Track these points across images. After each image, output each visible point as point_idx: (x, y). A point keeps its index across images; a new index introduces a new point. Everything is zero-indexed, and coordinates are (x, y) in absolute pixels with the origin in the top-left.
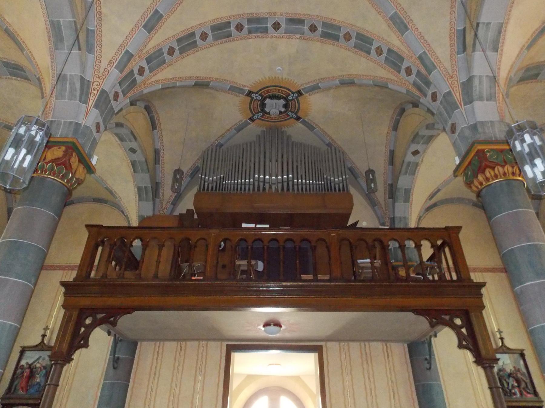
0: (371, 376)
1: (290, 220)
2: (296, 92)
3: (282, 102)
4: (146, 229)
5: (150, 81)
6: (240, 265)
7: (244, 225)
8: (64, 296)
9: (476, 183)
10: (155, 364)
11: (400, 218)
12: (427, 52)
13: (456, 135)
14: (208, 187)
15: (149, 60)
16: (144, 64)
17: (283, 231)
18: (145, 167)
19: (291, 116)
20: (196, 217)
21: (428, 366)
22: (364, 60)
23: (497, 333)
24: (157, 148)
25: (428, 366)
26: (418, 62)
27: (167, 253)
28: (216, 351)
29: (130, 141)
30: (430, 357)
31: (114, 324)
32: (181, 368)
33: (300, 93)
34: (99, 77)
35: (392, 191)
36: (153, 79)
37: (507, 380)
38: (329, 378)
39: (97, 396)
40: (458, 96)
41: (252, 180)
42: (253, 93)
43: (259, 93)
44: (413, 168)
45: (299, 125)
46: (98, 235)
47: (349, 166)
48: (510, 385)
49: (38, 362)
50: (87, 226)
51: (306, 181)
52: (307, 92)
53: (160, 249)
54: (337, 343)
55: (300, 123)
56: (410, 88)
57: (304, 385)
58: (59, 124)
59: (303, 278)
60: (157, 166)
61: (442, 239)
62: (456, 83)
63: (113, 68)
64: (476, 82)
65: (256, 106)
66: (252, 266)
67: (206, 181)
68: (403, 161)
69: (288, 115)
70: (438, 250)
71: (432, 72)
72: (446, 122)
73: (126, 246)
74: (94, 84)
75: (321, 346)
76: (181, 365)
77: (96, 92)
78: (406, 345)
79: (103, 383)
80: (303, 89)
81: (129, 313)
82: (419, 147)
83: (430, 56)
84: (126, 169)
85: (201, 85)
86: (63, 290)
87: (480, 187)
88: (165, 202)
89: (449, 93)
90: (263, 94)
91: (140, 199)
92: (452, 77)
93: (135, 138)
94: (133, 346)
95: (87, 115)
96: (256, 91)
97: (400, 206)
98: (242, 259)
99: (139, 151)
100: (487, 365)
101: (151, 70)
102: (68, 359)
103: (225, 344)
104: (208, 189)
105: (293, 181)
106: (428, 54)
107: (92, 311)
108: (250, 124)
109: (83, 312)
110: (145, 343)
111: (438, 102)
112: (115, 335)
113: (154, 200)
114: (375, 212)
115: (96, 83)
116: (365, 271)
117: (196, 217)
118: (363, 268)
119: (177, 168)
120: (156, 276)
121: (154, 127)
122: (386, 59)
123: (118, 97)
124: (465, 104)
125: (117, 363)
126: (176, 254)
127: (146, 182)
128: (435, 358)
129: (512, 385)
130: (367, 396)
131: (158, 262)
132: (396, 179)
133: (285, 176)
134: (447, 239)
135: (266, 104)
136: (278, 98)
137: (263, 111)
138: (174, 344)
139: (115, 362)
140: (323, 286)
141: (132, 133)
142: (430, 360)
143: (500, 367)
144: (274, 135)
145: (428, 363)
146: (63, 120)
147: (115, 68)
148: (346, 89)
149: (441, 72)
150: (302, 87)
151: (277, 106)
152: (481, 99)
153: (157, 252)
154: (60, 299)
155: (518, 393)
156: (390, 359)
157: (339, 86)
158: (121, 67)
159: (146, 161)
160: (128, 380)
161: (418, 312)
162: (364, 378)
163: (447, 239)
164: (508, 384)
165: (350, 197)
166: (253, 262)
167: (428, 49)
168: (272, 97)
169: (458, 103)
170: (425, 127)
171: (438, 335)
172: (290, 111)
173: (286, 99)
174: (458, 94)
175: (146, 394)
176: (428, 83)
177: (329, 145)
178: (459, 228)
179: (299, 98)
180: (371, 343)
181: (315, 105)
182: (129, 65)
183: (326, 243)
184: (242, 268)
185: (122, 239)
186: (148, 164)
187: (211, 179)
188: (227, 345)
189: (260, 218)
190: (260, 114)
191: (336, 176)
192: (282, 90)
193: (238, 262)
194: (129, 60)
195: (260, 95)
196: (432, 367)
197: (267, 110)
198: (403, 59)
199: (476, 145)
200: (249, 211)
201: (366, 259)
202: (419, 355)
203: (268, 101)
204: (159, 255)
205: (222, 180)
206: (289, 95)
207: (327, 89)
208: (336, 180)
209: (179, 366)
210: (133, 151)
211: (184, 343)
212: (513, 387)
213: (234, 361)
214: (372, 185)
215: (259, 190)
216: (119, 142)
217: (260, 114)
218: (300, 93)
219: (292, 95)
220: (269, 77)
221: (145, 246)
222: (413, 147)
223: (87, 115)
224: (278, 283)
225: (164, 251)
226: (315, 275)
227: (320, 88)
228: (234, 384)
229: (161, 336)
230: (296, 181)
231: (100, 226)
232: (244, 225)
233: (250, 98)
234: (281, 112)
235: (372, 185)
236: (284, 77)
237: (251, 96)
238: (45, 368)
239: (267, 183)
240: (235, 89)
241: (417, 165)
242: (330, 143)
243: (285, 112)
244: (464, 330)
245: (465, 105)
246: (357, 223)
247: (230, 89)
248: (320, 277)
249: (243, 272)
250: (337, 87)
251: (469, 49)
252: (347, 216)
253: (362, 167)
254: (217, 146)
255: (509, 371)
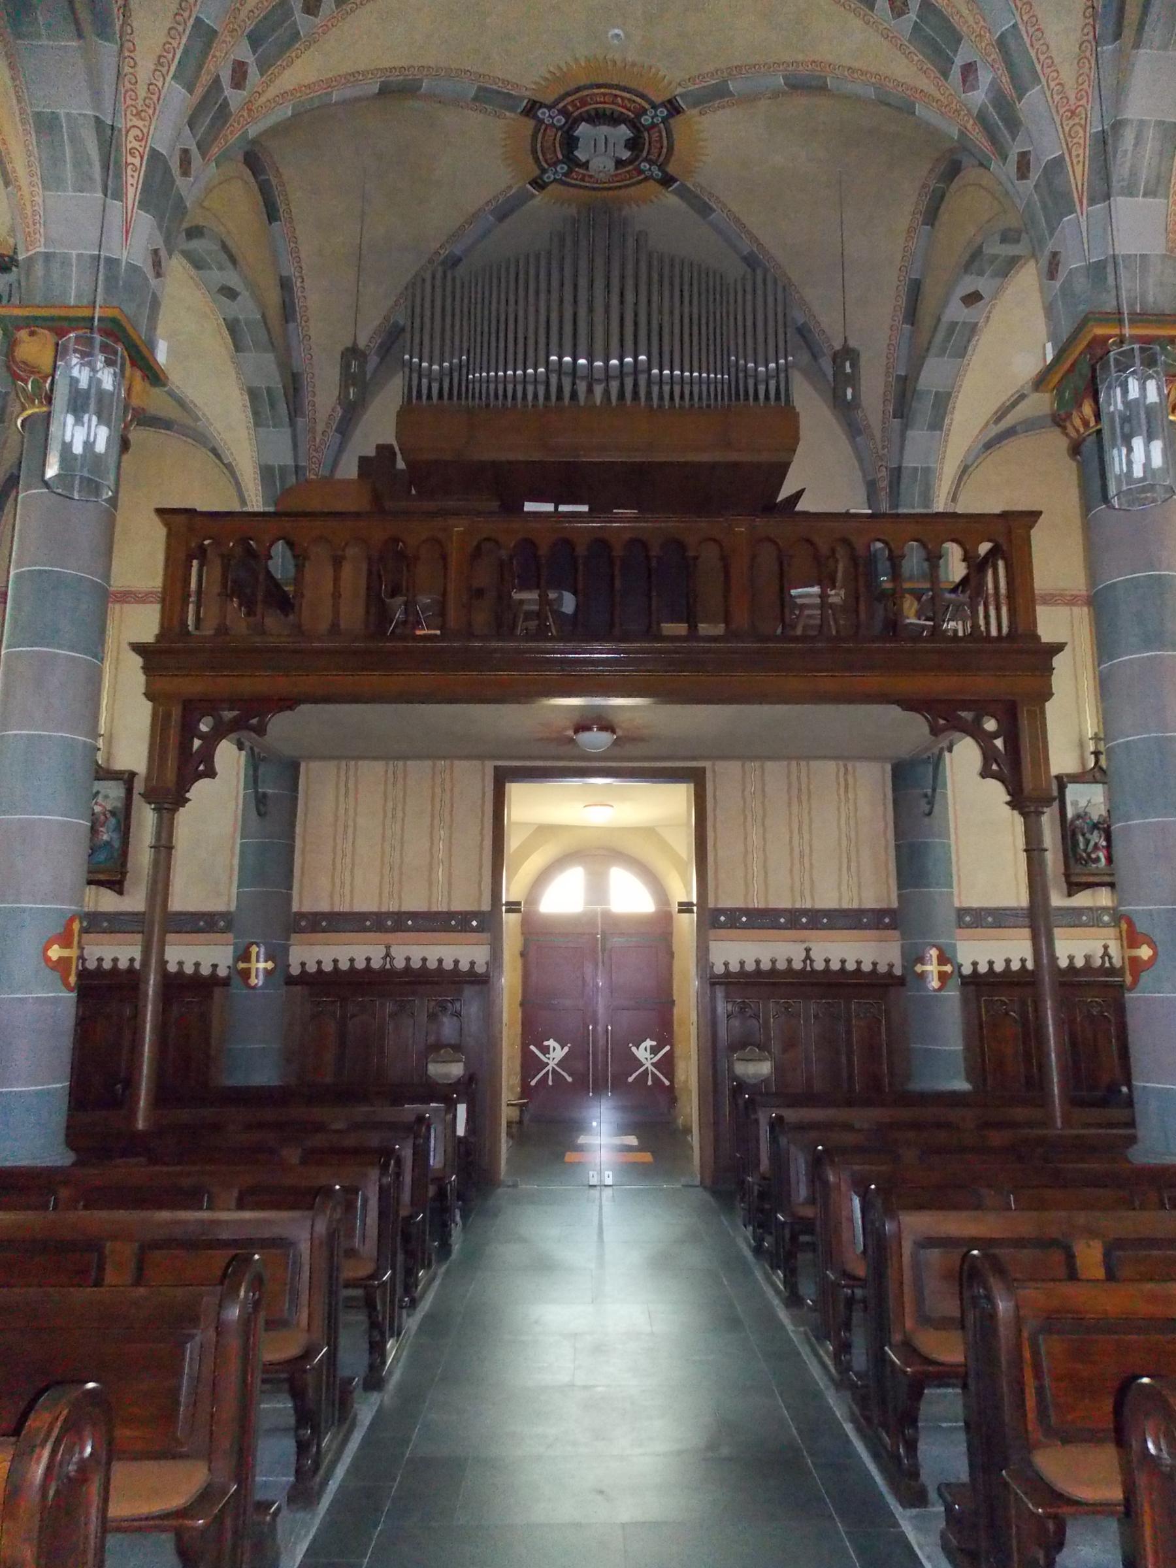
0: (805, 827)
1: (637, 483)
2: (663, 105)
3: (624, 131)
4: (295, 514)
5: (263, 99)
6: (521, 602)
7: (529, 507)
8: (145, 673)
9: (1077, 422)
10: (342, 806)
11: (916, 469)
12: (1022, 28)
13: (1057, 284)
14: (430, 388)
15: (255, 40)
16: (244, 52)
17: (623, 521)
18: (263, 336)
19: (648, 173)
20: (401, 464)
21: (927, 808)
22: (856, 23)
23: (1091, 743)
24: (285, 274)
25: (927, 808)
26: (995, 55)
27: (353, 576)
28: (473, 779)
29: (221, 268)
30: (934, 790)
31: (261, 730)
32: (400, 814)
33: (674, 108)
34: (138, 114)
35: (904, 398)
36: (272, 92)
37: (1088, 835)
38: (715, 831)
39: (232, 869)
40: (1078, 174)
41: (541, 370)
42: (542, 105)
43: (561, 105)
44: (961, 340)
45: (670, 199)
46: (189, 531)
47: (801, 321)
48: (1092, 844)
49: (96, 803)
50: (160, 512)
51: (682, 372)
52: (695, 105)
53: (337, 562)
54: (739, 763)
55: (673, 192)
56: (969, 126)
57: (665, 847)
58: (65, 261)
59: (665, 633)
60: (291, 326)
61: (989, 541)
62: (1081, 134)
63: (168, 79)
64: (1129, 135)
65: (550, 144)
66: (549, 603)
67: (425, 372)
68: (939, 320)
69: (640, 172)
70: (977, 567)
71: (1027, 90)
72: (1041, 242)
73: (253, 558)
74: (131, 137)
75: (704, 770)
76: (400, 807)
77: (137, 161)
78: (889, 767)
79: (242, 844)
80: (681, 95)
81: (290, 708)
82: (981, 284)
83: (1027, 40)
84: (217, 343)
85: (397, 90)
86: (138, 661)
87: (1082, 430)
88: (320, 428)
89: (1058, 162)
90: (570, 108)
91: (258, 420)
92: (1073, 113)
93: (233, 260)
94: (292, 769)
95: (127, 232)
96: (549, 99)
97: (917, 436)
98: (524, 587)
99: (245, 294)
100: (1032, 809)
101: (264, 66)
102: (181, 800)
103: (490, 765)
104: (429, 397)
105: (650, 374)
106: (1024, 33)
107: (208, 705)
108: (533, 196)
109: (192, 709)
110: (315, 765)
111: (1030, 183)
112: (252, 749)
113: (292, 424)
114: (856, 449)
115: (134, 132)
116: (807, 612)
117: (401, 464)
118: (803, 607)
119: (349, 345)
120: (334, 628)
121: (272, 213)
122: (916, 28)
123: (190, 163)
124: (1092, 201)
125: (265, 805)
126: (373, 578)
127: (271, 377)
128: (945, 796)
129: (1096, 844)
130: (792, 865)
131: (334, 596)
132: (917, 363)
133: (629, 360)
134: (1004, 538)
135: (578, 139)
136: (614, 120)
137: (572, 162)
138: (379, 766)
139: (260, 803)
140: (709, 651)
141: (225, 247)
142: (933, 796)
143: (1081, 811)
144: (599, 226)
145: (928, 803)
146: (74, 252)
147: (174, 77)
148: (802, 101)
149: (1048, 94)
150: (680, 90)
151: (610, 145)
152: (1130, 191)
153: (329, 572)
154: (138, 680)
155: (1103, 860)
156: (851, 795)
157: (784, 93)
158: (187, 76)
159: (263, 316)
160: (292, 837)
161: (909, 704)
162: (791, 832)
163: (1004, 538)
164: (1087, 842)
165: (789, 417)
166: (552, 595)
167: (1025, 18)
168: (596, 118)
169: (1075, 195)
170: (997, 237)
171: (955, 748)
172: (646, 160)
173: (634, 125)
174: (1079, 169)
175: (334, 864)
176: (1013, 124)
177: (751, 261)
178: (1035, 515)
179: (671, 121)
180: (811, 763)
181: (716, 143)
182: (210, 66)
183: (721, 547)
184: (526, 607)
185: (244, 541)
186: (269, 327)
187: (435, 367)
188: (496, 768)
189: (563, 481)
190: (562, 168)
191: (761, 359)
192: (623, 98)
193: (517, 596)
194: (208, 45)
195: (561, 112)
196: (936, 808)
197: (581, 155)
198: (959, 41)
199: (1090, 323)
200: (536, 456)
201: (812, 586)
202: (913, 789)
203: (583, 129)
204: (336, 579)
205: (464, 371)
206: (645, 112)
207: (749, 99)
208: (762, 369)
209: (394, 809)
210: (230, 293)
211: (401, 763)
212: (1096, 847)
213: (510, 799)
214: (849, 392)
215: (560, 397)
216: (193, 272)
217: (562, 168)
218: (674, 108)
219: (651, 112)
220: (587, 60)
221: (300, 558)
222: (969, 284)
223: (127, 232)
224: (608, 646)
225: (347, 570)
226: (693, 627)
227: (730, 94)
228: (513, 843)
229: (348, 751)
230: (655, 371)
231: (190, 512)
232: (529, 507)
233: (531, 123)
234: (619, 163)
235: (849, 392)
236: (630, 59)
237: (535, 117)
238: (113, 813)
239: (582, 378)
240: (489, 97)
241: (973, 329)
242: (752, 253)
243: (630, 161)
244: (999, 743)
245: (1091, 204)
246: (799, 495)
247: (476, 99)
248: (704, 628)
249: (528, 616)
250: (776, 95)
251: (1128, 33)
252: (780, 471)
253: (831, 328)
254: (443, 263)
255: (1095, 818)
